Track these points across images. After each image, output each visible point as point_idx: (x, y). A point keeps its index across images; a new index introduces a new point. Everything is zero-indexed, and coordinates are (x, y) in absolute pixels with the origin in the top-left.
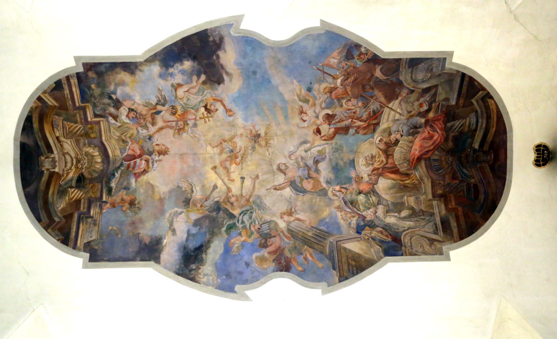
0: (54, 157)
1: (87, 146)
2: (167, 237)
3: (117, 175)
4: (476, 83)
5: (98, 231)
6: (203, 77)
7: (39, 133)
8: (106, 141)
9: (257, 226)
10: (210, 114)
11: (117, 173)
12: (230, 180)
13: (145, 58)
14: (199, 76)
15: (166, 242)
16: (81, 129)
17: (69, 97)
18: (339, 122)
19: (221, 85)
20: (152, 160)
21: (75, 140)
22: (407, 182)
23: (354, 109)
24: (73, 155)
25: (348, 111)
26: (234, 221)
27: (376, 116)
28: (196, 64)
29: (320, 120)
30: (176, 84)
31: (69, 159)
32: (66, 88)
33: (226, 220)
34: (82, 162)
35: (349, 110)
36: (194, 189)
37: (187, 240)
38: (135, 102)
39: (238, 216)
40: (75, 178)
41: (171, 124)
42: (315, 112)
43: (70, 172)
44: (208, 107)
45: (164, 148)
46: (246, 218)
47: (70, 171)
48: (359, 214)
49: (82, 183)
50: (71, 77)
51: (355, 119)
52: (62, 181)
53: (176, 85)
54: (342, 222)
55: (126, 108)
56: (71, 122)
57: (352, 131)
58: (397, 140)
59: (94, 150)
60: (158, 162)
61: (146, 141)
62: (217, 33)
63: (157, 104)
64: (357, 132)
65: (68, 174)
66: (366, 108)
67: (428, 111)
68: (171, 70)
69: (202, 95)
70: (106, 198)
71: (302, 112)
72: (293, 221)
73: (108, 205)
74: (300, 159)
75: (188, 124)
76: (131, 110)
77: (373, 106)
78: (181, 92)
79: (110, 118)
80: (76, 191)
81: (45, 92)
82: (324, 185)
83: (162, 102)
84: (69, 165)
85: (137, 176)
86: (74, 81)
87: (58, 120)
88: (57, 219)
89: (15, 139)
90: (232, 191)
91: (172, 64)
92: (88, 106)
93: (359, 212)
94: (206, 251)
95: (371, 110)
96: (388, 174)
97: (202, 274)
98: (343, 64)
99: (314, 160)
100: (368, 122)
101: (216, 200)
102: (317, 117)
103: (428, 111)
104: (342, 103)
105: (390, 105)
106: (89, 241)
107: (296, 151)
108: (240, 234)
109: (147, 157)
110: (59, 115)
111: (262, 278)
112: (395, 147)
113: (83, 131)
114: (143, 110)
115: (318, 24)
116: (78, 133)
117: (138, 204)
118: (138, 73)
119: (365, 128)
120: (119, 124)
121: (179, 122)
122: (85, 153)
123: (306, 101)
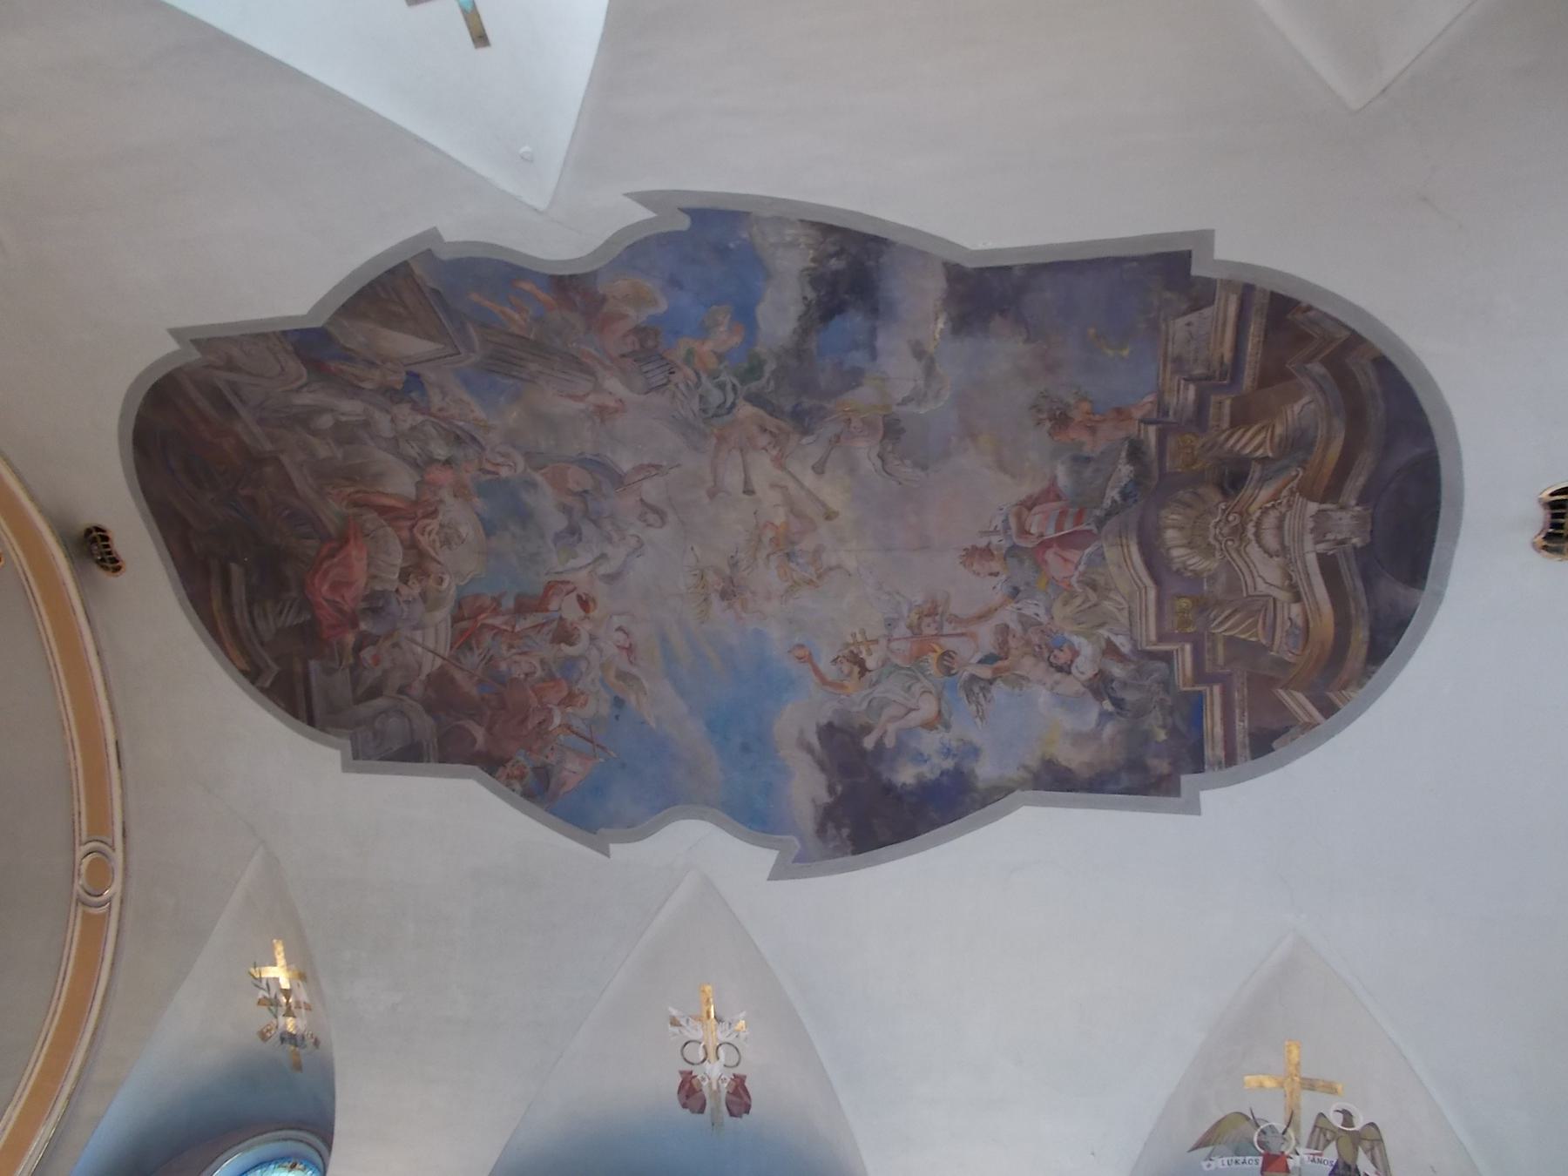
0: (1317, 543)
1: (1205, 575)
2: (938, 336)
3: (1113, 494)
4: (283, 705)
5: (1167, 340)
6: (869, 743)
7: (1353, 612)
8: (1146, 587)
9: (677, 378)
10: (852, 652)
11: (1114, 501)
12: (781, 487)
13: (1010, 797)
14: (879, 743)
15: (936, 324)
16: (1216, 622)
17: (1237, 711)
18: (543, 625)
19: (824, 721)
20: (1010, 536)
21: (1242, 591)
22: (352, 490)
23: (515, 654)
24: (1254, 550)
25: (526, 649)
26: (746, 388)
27: (464, 640)
28: (885, 776)
29: (585, 628)
30: (937, 729)
31: (1270, 540)
32: (1241, 736)
33: (769, 390)
34: (1226, 530)
35: (524, 653)
36: (879, 463)
37: (873, 333)
38: (1052, 689)
39: (737, 401)
40: (1252, 484)
41: (954, 629)
42: (600, 650)
43: (1268, 502)
44: (856, 669)
45: (976, 567)
46: (715, 397)
47: (1269, 505)
48: (431, 415)
49: (1227, 473)
50: (1220, 763)
51: (506, 630)
52: (1297, 475)
53: (939, 726)
54: (466, 397)
55: (1078, 675)
56: (1244, 640)
57: (509, 603)
58: (406, 583)
59: (1184, 562)
60: (992, 529)
61: (1028, 584)
62: (831, 845)
63: (991, 682)
64: (497, 601)
65: (1275, 497)
66: (488, 657)
67: (358, 648)
68: (949, 764)
69: (874, 698)
70: (1146, 432)
71: (629, 650)
72: (588, 394)
73: (1138, 414)
74: (616, 537)
75: (910, 627)
76: (1065, 669)
77: (473, 659)
78: (928, 708)
79: (1126, 648)
80: (1247, 451)
81: (1310, 726)
82: (538, 477)
83: (976, 687)
84: (1270, 521)
85: (1051, 493)
86: (1214, 750)
87: (1285, 648)
88: (1317, 368)
89: (1439, 597)
90: (772, 460)
91: (945, 779)
92: (1184, 685)
93: (432, 419)
94: (808, 306)
95: (477, 652)
96: (400, 505)
97: (802, 246)
98: (552, 759)
99: (580, 534)
100: (479, 624)
101: (809, 439)
102: (593, 638)
103: (358, 648)
104: (544, 670)
105: (439, 662)
106: (1196, 314)
107: (628, 555)
108: (720, 357)
109: (1022, 543)
110: (1282, 664)
111: (620, 255)
112: (404, 565)
113: (1212, 616)
114: (1028, 665)
115: (613, 847)
116: (1227, 613)
117: (1041, 420)
118: (1033, 762)
119: (482, 610)
120: (1104, 632)
121: (934, 632)
122: (1214, 556)
123: (623, 676)
